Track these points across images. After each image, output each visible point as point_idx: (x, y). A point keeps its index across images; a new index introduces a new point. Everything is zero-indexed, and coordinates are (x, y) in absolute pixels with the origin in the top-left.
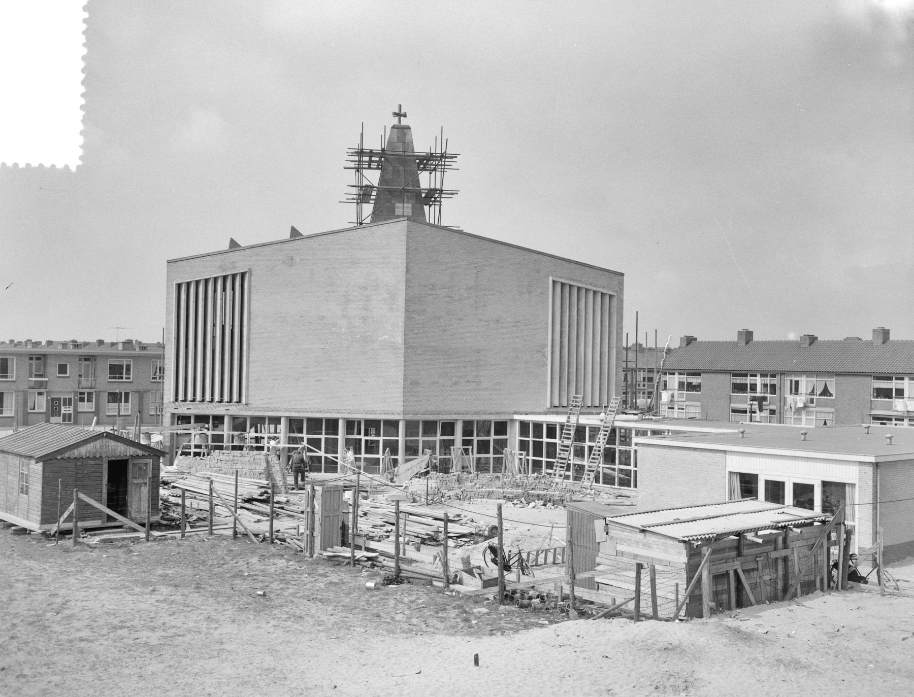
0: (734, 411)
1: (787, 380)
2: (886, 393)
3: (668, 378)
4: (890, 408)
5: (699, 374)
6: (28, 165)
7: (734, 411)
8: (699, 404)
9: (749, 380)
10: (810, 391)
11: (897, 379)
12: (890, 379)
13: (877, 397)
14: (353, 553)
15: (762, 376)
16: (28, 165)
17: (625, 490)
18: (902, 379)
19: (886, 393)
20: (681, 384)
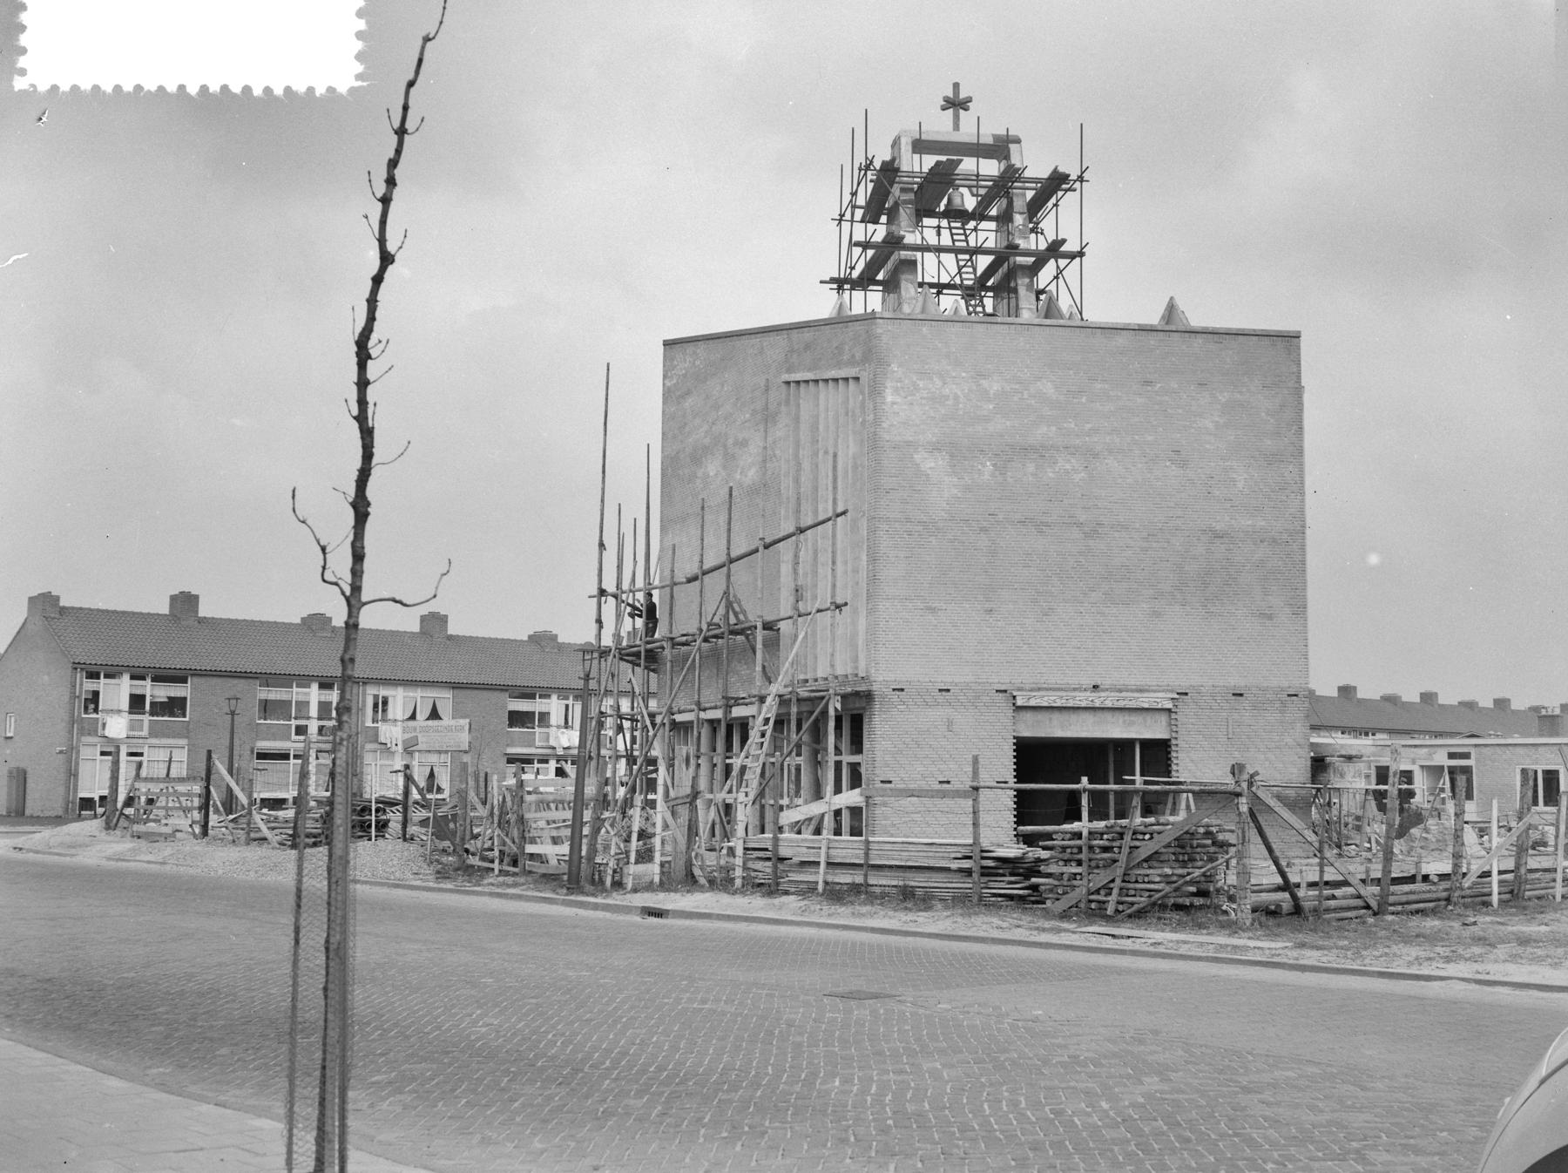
0: (262, 756)
1: (371, 691)
2: (517, 719)
3: (102, 684)
4: (531, 744)
5: (183, 680)
6: (331, 90)
7: (262, 756)
8: (183, 742)
9: (537, 706)
10: (409, 714)
11: (106, 676)
12: (532, 696)
13: (511, 725)
14: (866, 876)
15: (323, 686)
16: (331, 90)
17: (1385, 761)
18: (548, 696)
19: (517, 719)
20: (137, 702)
